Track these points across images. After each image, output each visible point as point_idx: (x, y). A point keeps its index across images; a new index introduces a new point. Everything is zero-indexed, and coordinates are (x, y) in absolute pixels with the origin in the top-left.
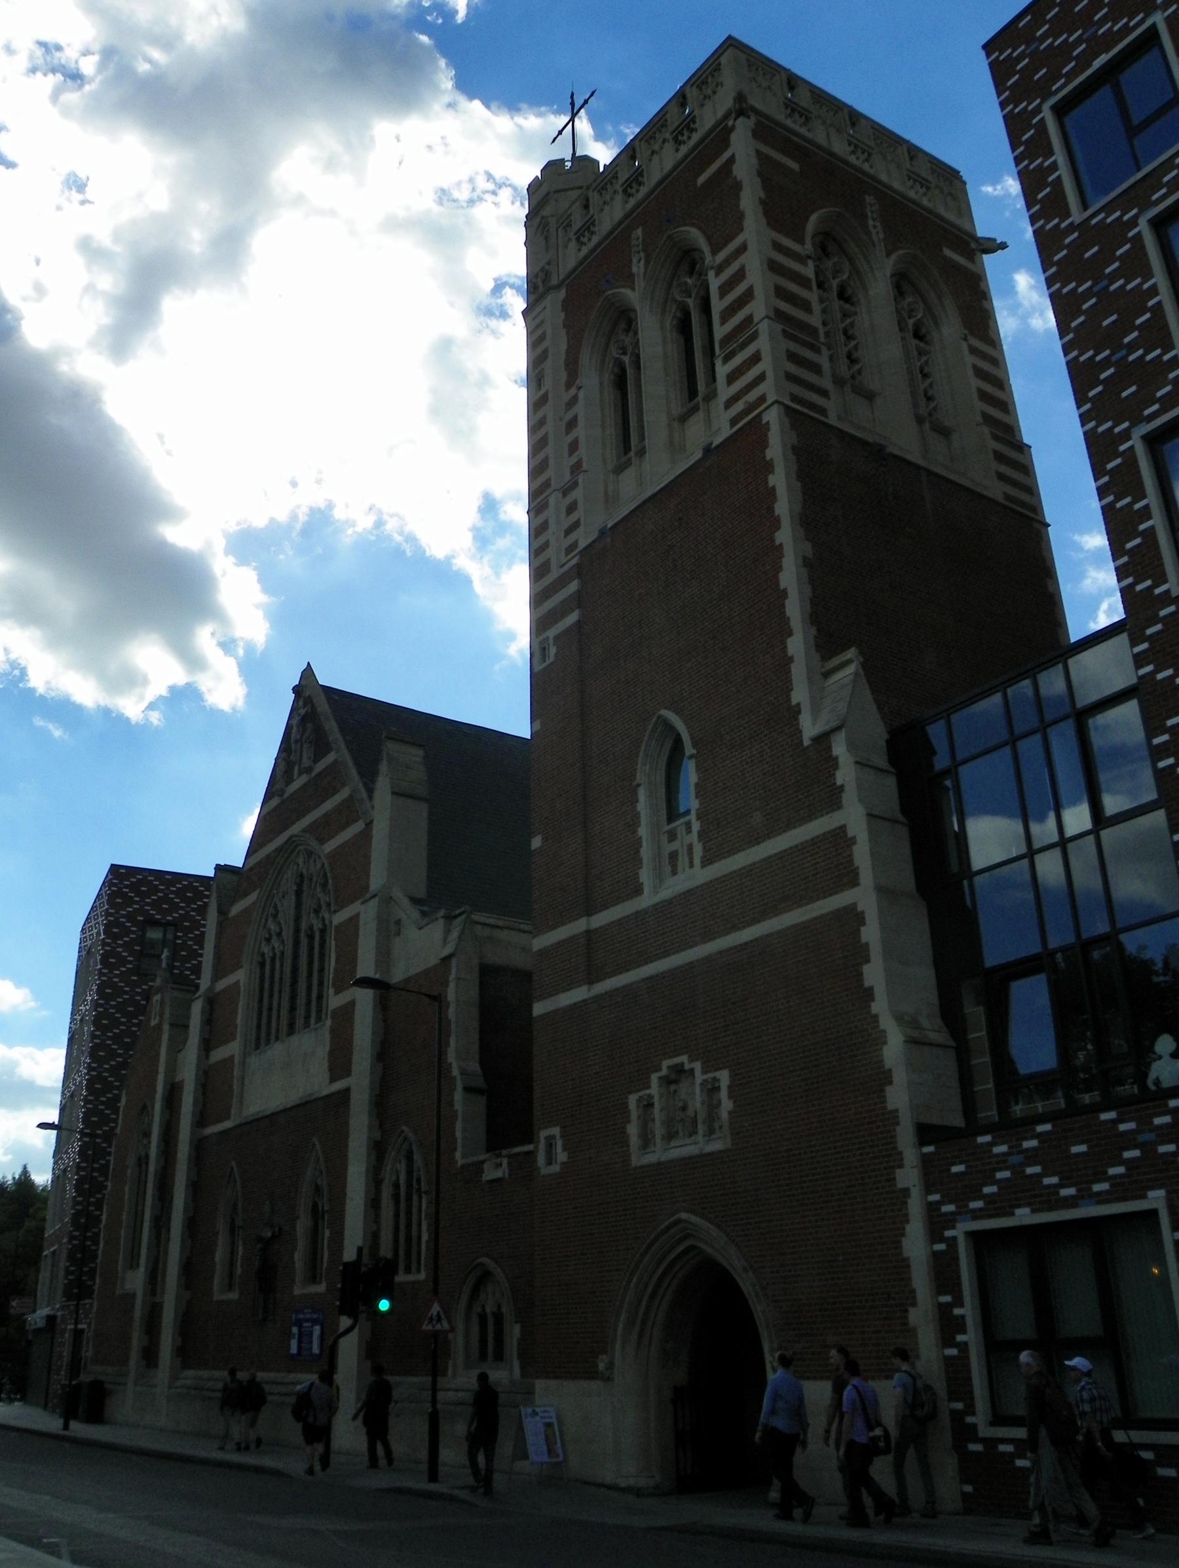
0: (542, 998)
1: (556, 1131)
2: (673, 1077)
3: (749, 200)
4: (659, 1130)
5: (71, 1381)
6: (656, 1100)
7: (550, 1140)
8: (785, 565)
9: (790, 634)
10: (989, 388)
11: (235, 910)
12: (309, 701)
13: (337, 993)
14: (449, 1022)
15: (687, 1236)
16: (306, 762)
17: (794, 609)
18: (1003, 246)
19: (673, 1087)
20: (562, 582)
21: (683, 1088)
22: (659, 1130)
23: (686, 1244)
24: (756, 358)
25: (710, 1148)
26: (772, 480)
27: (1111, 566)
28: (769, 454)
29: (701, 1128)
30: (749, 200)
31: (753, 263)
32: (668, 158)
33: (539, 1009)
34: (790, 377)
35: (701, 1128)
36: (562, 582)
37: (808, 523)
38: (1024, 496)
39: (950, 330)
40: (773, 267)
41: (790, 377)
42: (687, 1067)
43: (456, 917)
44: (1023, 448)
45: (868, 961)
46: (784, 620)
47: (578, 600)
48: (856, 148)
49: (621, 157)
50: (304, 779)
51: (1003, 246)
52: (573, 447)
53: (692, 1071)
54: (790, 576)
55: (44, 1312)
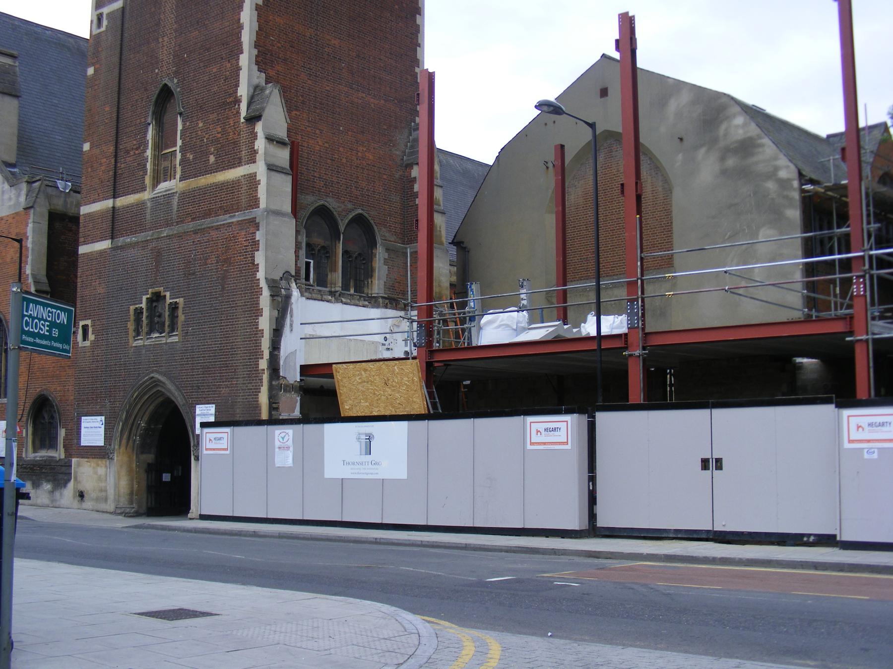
0: (85, 243)
1: (89, 322)
2: (154, 298)
6: (144, 310)
7: (85, 328)
8: (244, 8)
9: (242, 53)
14: (27, 248)
15: (156, 385)
17: (247, 37)
18: (627, 24)
19: (154, 304)
23: (155, 390)
25: (170, 340)
27: (798, 235)
29: (167, 329)
33: (83, 249)
35: (167, 329)
42: (162, 294)
43: (34, 182)
45: (258, 250)
46: (239, 44)
49: (836, 139)
51: (627, 24)
53: (165, 296)
55: (46, 417)
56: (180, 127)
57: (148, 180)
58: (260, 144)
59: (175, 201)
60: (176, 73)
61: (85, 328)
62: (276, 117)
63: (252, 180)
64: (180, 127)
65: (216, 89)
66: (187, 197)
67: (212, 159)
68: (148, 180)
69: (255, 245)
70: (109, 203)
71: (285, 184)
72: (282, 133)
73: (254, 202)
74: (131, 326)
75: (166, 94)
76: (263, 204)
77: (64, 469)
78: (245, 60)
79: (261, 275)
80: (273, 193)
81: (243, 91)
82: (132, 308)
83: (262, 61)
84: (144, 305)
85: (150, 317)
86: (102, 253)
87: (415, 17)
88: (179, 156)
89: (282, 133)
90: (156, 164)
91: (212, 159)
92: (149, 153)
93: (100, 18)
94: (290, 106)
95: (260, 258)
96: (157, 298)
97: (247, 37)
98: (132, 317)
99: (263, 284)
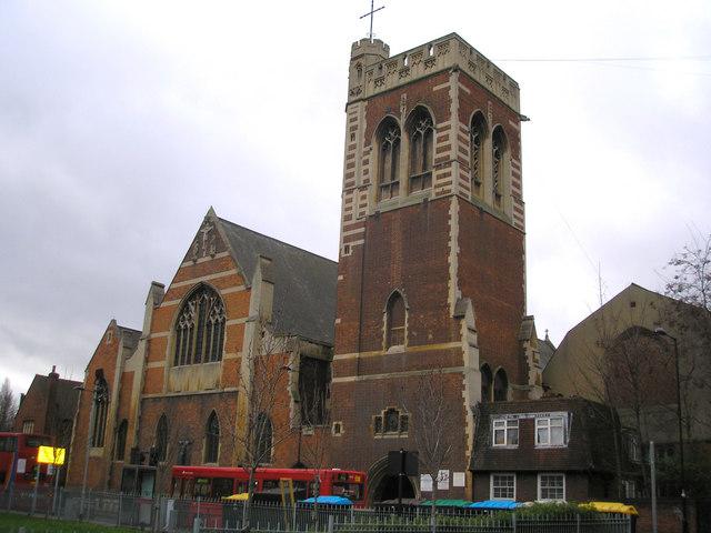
3: (454, 107)
4: (403, 176)
5: (151, 332)
7: (337, 427)
10: (516, 180)
11: (164, 304)
12: (213, 232)
13: (227, 352)
16: (212, 252)
17: (453, 270)
20: (357, 226)
21: (393, 417)
22: (403, 176)
24: (449, 174)
26: (450, 244)
28: (450, 213)
30: (454, 107)
31: (453, 133)
32: (418, 72)
33: (336, 357)
34: (460, 184)
36: (357, 226)
37: (460, 241)
38: (520, 223)
39: (507, 155)
40: (459, 138)
41: (460, 184)
44: (522, 203)
47: (363, 236)
48: (488, 77)
50: (209, 258)
52: (366, 172)
54: (453, 259)
56: (407, 317)
57: (383, 344)
58: (464, 331)
59: (404, 359)
60: (404, 286)
61: (337, 427)
62: (470, 319)
63: (459, 352)
64: (407, 317)
65: (431, 297)
66: (410, 356)
67: (430, 336)
68: (383, 344)
69: (463, 387)
70: (357, 355)
71: (476, 353)
72: (473, 326)
73: (461, 363)
74: (372, 426)
75: (396, 296)
76: (466, 364)
77: (314, 413)
78: (453, 283)
79: (467, 404)
80: (471, 359)
81: (452, 300)
82: (373, 417)
83: (461, 284)
84: (382, 415)
85: (386, 422)
86: (350, 383)
87: (276, 311)
88: (406, 333)
89: (473, 326)
90: (389, 335)
91: (430, 336)
92: (384, 329)
93: (347, 249)
94: (476, 308)
95: (465, 394)
96: (392, 411)
97: (453, 270)
98: (373, 422)
99: (468, 409)
